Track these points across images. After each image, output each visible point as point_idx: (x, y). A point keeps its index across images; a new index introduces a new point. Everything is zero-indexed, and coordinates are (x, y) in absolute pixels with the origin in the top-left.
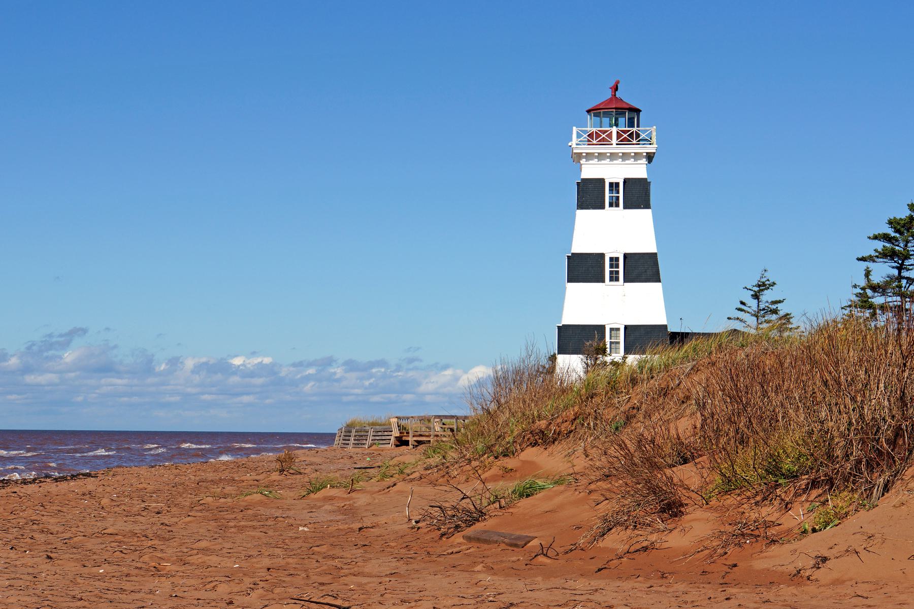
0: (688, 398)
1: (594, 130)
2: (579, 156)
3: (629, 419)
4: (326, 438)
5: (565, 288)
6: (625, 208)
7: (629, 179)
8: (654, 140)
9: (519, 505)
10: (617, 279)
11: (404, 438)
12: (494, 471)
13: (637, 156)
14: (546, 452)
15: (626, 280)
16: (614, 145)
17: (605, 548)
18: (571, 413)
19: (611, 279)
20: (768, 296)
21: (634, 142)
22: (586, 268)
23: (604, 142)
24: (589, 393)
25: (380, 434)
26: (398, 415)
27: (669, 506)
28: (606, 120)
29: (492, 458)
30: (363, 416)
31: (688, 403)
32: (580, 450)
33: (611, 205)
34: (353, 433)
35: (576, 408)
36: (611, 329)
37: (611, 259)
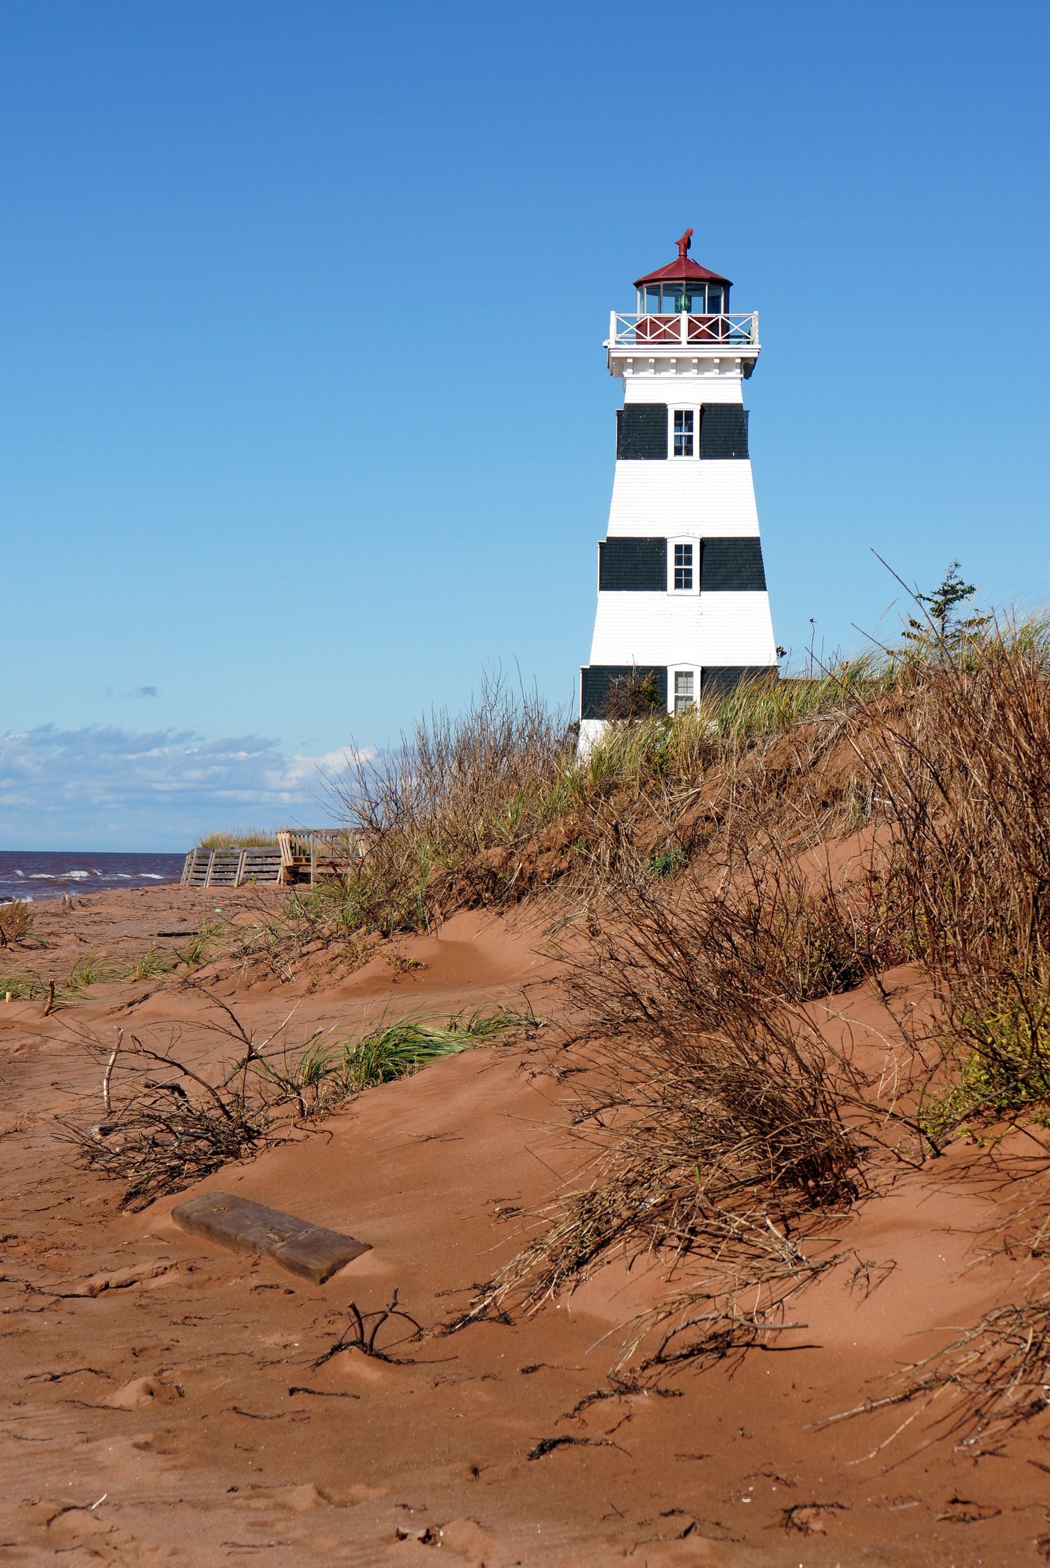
0: (836, 794)
1: (648, 316)
2: (622, 363)
3: (693, 845)
4: (169, 864)
5: (595, 601)
6: (703, 456)
7: (710, 405)
8: (755, 336)
9: (355, 1107)
10: (688, 585)
11: (301, 870)
12: (376, 966)
13: (724, 364)
14: (502, 922)
15: (705, 586)
16: (684, 345)
17: (581, 1316)
18: (559, 831)
19: (678, 585)
20: (961, 611)
21: (720, 339)
22: (632, 564)
23: (666, 338)
24: (606, 779)
25: (259, 861)
26: (290, 828)
27: (812, 1168)
28: (669, 301)
29: (376, 934)
30: (233, 826)
31: (838, 806)
32: (580, 918)
33: (678, 452)
34: (212, 860)
35: (571, 819)
36: (678, 675)
37: (678, 548)
